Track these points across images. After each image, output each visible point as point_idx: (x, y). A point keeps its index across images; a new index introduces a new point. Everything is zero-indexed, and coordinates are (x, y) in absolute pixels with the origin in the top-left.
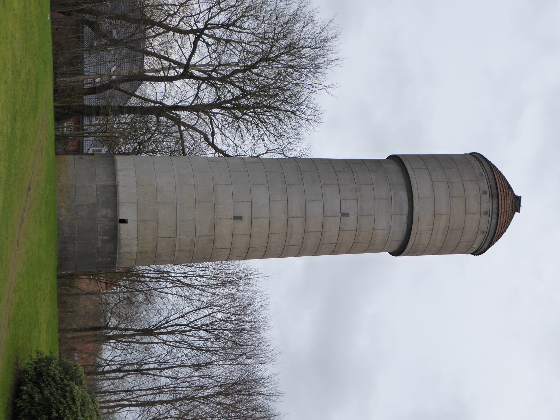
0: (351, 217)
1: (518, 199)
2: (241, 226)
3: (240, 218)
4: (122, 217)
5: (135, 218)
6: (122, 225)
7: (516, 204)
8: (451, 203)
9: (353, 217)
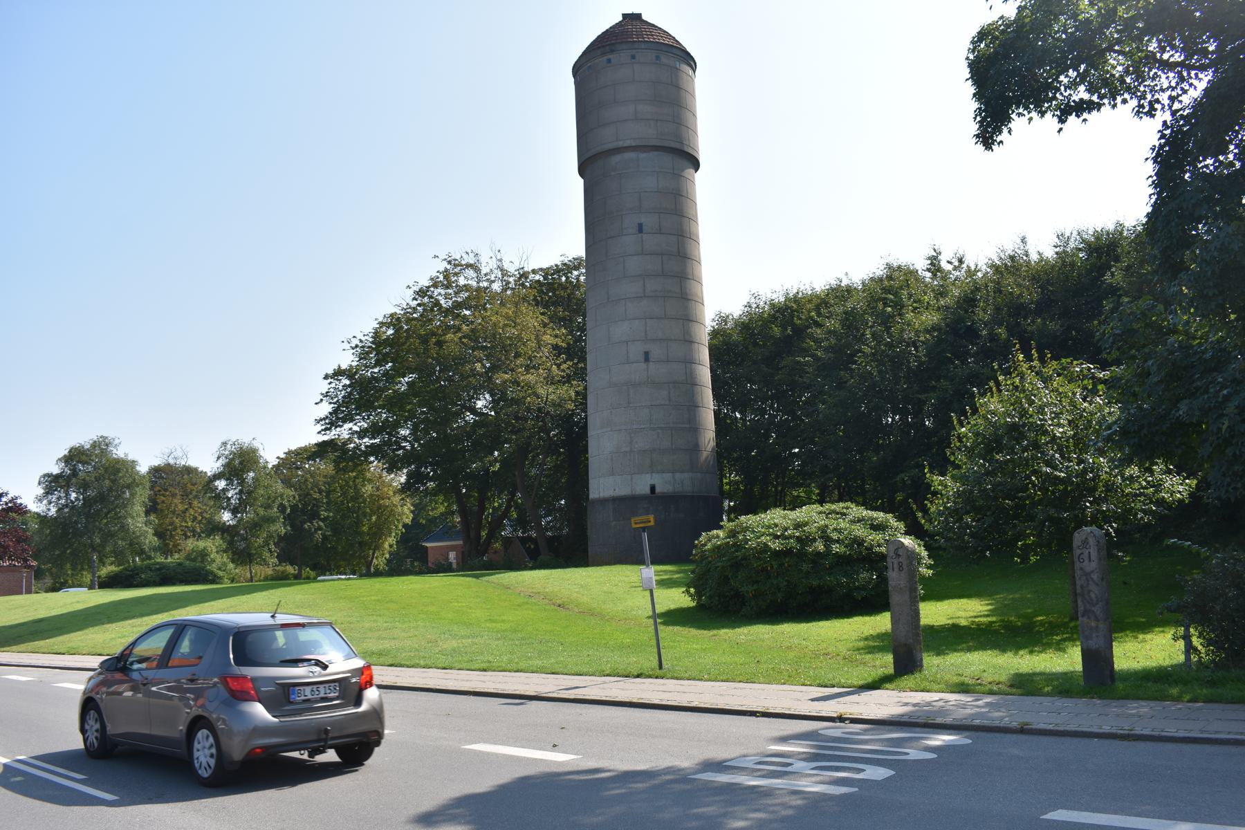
0: (643, 220)
1: (625, 16)
2: (656, 351)
3: (647, 354)
4: (647, 490)
5: (648, 476)
6: (658, 490)
7: (633, 19)
8: (633, 102)
9: (643, 219)
